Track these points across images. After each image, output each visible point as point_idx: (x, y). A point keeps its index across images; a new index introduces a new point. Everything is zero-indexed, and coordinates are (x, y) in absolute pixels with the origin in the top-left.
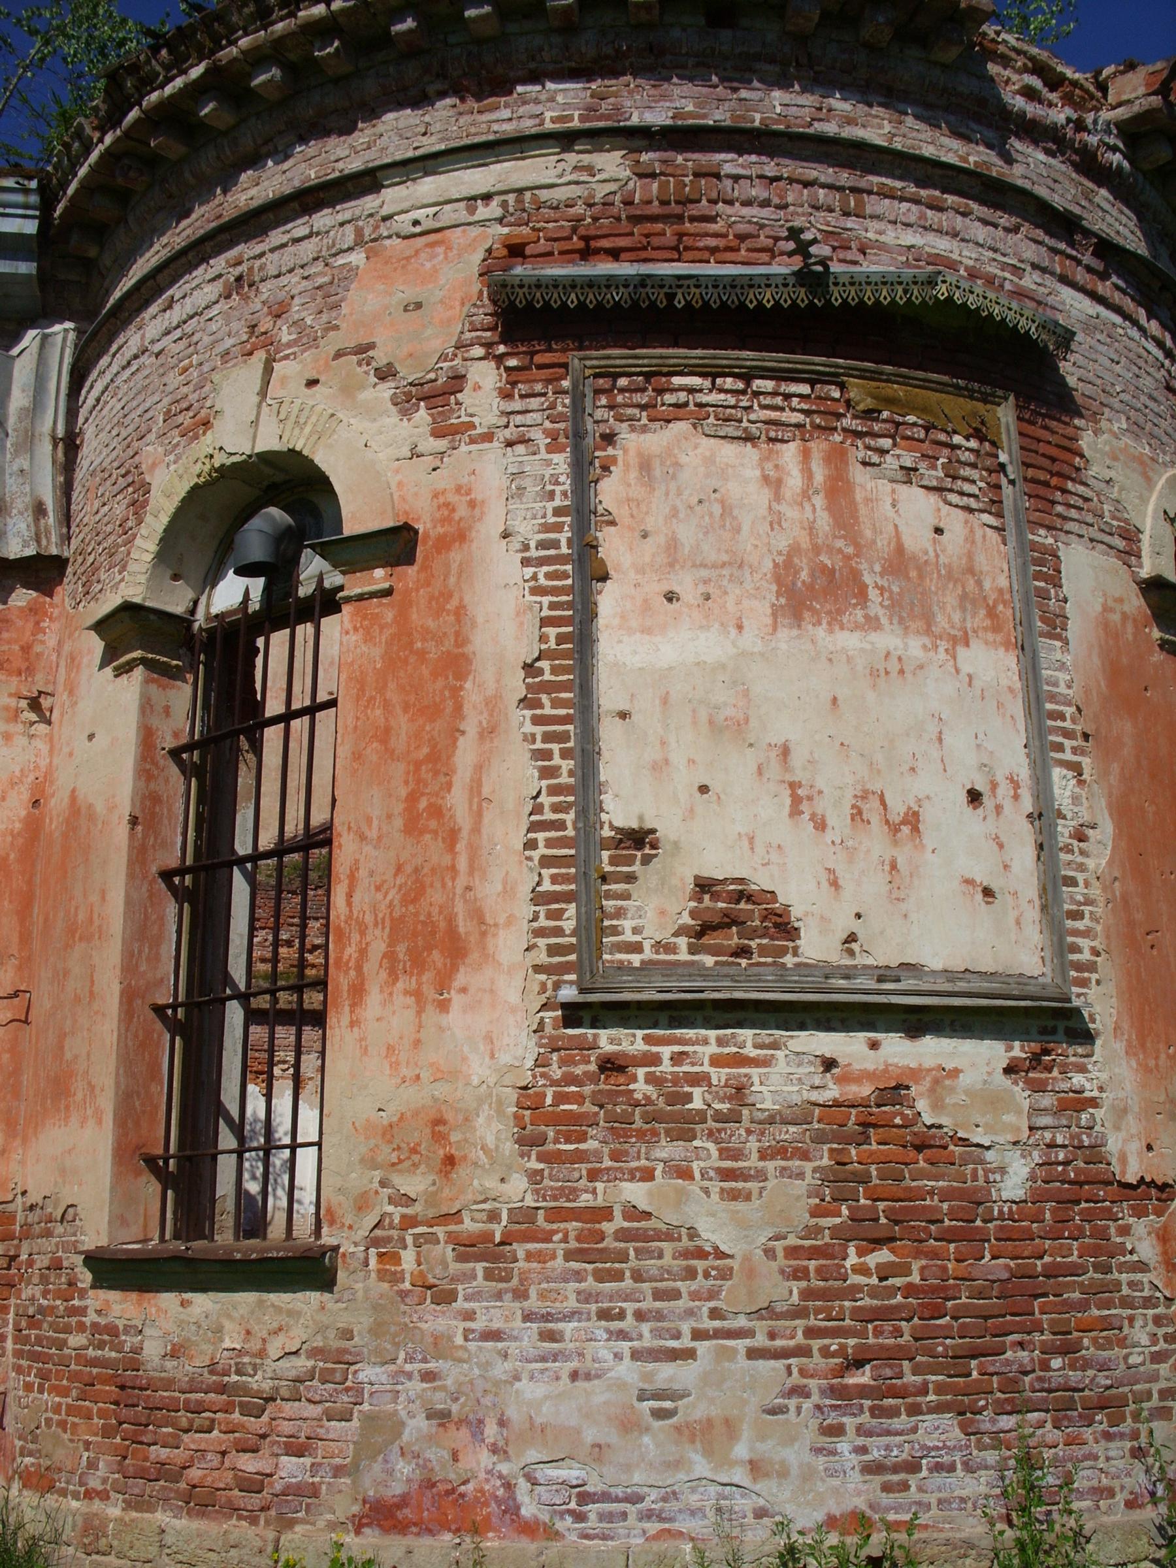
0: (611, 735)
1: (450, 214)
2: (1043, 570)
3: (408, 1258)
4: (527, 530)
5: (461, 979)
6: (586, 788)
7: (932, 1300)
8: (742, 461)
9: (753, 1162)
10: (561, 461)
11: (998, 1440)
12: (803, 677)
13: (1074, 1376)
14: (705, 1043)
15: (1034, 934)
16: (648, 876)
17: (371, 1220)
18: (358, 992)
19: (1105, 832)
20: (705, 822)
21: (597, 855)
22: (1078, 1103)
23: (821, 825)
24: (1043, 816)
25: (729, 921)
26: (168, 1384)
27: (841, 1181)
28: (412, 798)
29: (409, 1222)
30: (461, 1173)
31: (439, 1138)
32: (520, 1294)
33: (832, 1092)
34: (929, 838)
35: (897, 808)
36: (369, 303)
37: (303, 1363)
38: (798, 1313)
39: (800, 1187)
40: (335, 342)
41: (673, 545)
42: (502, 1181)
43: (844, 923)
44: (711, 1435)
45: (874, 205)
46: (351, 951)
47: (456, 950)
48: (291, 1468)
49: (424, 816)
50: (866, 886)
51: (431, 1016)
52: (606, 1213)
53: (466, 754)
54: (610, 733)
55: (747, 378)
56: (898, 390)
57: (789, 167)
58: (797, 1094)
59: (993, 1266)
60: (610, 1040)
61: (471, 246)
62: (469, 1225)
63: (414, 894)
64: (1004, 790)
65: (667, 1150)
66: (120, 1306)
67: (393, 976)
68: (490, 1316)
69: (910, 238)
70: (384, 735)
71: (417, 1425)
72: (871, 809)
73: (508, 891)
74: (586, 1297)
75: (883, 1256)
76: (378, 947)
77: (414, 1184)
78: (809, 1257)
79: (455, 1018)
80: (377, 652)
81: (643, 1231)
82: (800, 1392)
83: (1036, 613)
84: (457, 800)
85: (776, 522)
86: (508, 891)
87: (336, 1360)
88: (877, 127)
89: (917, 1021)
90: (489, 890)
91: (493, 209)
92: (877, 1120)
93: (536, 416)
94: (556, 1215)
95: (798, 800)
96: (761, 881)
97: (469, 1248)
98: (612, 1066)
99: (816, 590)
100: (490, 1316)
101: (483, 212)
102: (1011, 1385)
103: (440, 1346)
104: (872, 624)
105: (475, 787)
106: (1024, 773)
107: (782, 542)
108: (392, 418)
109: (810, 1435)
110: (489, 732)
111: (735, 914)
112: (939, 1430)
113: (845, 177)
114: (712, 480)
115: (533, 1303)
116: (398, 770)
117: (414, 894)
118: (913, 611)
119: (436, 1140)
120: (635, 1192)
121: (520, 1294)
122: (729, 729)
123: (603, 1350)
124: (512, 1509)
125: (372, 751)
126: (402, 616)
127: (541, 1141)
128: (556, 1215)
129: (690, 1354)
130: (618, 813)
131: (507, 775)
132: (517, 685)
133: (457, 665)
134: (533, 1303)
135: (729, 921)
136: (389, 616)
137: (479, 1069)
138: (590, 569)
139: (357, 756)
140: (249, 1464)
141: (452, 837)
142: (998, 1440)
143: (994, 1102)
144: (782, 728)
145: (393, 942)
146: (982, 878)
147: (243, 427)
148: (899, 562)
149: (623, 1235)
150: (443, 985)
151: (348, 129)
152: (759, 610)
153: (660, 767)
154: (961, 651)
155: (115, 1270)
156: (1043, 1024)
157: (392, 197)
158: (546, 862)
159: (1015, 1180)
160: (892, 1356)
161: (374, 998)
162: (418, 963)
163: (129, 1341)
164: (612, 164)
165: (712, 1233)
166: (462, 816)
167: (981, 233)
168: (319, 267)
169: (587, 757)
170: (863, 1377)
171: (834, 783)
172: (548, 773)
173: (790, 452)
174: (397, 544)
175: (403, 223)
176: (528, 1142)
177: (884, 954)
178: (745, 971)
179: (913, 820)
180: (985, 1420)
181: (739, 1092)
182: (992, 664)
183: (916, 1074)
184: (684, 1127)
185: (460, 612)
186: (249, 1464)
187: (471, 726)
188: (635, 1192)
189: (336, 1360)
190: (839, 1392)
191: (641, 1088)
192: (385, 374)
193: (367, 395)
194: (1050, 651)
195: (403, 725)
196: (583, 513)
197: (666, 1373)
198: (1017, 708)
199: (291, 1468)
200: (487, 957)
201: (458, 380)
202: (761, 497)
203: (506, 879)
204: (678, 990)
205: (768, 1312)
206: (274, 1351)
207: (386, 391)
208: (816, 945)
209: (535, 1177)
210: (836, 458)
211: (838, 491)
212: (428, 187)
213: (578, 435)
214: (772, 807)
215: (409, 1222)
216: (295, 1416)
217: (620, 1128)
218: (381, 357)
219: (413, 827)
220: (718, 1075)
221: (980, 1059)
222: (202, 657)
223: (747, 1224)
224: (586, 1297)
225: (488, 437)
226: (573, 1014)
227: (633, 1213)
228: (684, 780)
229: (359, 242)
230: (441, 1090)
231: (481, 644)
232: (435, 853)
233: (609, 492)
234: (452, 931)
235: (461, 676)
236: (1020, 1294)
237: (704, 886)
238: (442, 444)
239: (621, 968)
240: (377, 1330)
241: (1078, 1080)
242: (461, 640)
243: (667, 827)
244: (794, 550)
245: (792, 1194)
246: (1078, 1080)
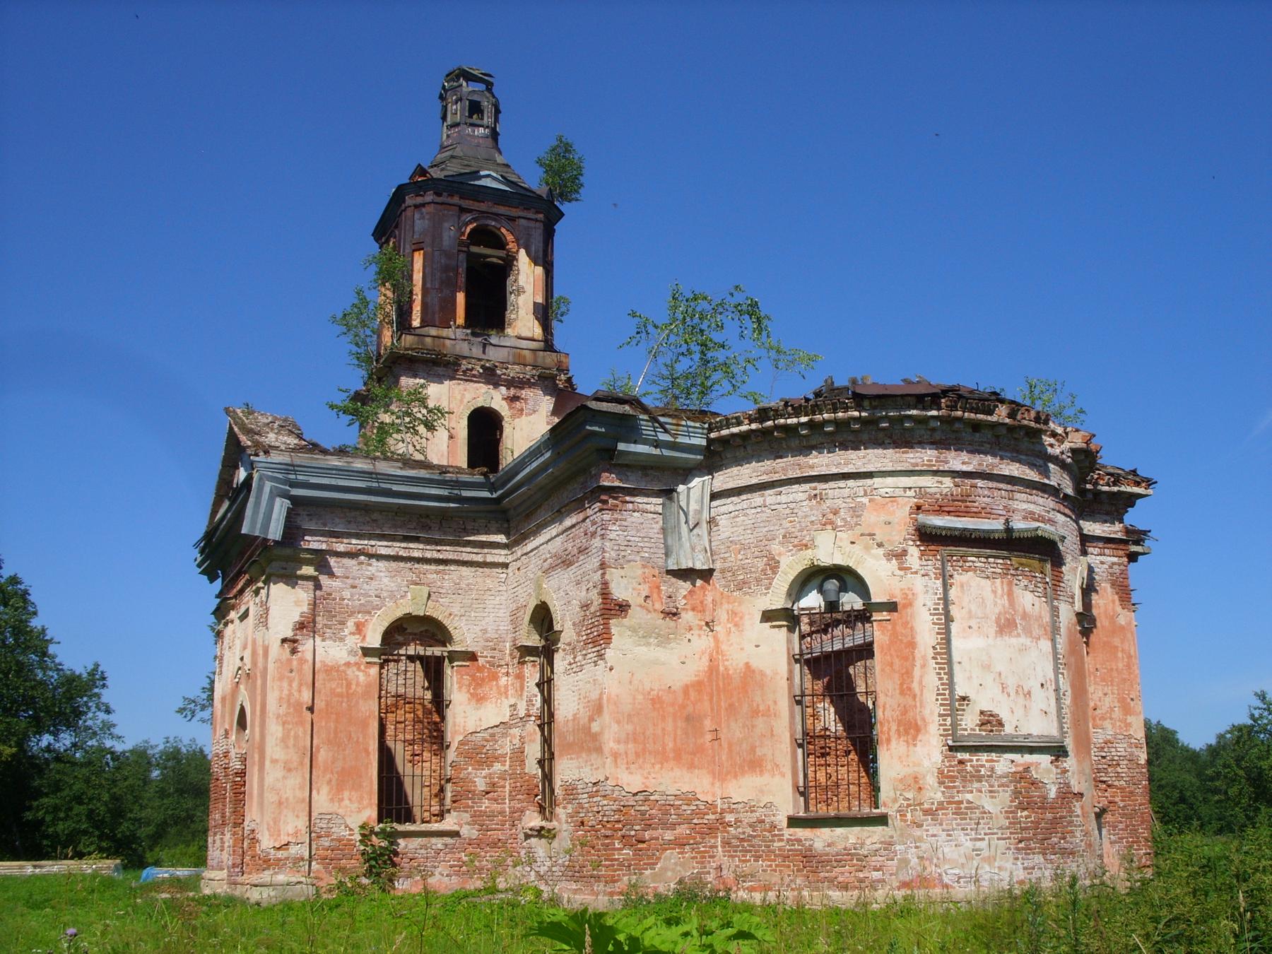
1: (899, 492)
2: (1055, 611)
3: (909, 815)
4: (930, 604)
5: (920, 737)
6: (951, 685)
7: (1036, 824)
9: (996, 788)
10: (939, 583)
11: (1051, 862)
12: (1004, 650)
13: (1066, 846)
14: (984, 757)
15: (1055, 724)
17: (897, 805)
18: (889, 740)
19: (1069, 693)
20: (984, 695)
21: (955, 704)
22: (1065, 771)
24: (1057, 690)
25: (989, 722)
26: (827, 855)
27: (1016, 793)
28: (901, 684)
29: (909, 805)
30: (923, 792)
31: (916, 782)
32: (941, 824)
33: (1014, 770)
35: (1026, 690)
36: (871, 518)
37: (878, 846)
38: (1008, 828)
39: (1007, 795)
40: (858, 530)
41: (970, 612)
42: (935, 794)
44: (990, 860)
45: (1017, 496)
46: (885, 729)
47: (918, 730)
48: (876, 875)
49: (905, 690)
50: (1019, 712)
51: (911, 748)
52: (961, 802)
53: (917, 672)
54: (956, 668)
56: (1024, 560)
57: (995, 485)
58: (1006, 770)
59: (1049, 816)
60: (960, 756)
61: (905, 505)
62: (926, 806)
63: (904, 712)
65: (976, 785)
66: (801, 833)
67: (899, 736)
68: (933, 830)
69: (1025, 506)
70: (891, 664)
71: (914, 861)
73: (932, 713)
74: (958, 825)
75: (1025, 813)
76: (894, 727)
77: (910, 795)
78: (1010, 813)
79: (918, 749)
80: (887, 638)
81: (971, 807)
82: (1009, 849)
84: (915, 686)
86: (932, 713)
87: (888, 845)
88: (1014, 469)
89: (1032, 750)
90: (927, 712)
91: (912, 493)
92: (1023, 778)
93: (932, 565)
94: (949, 803)
95: (1004, 688)
96: (996, 711)
97: (926, 812)
98: (961, 762)
99: (1006, 626)
100: (933, 830)
101: (909, 493)
102: (1053, 848)
103: (920, 839)
104: (1019, 635)
105: (920, 682)
107: (997, 611)
108: (884, 561)
109: (1011, 860)
110: (923, 666)
111: (990, 720)
112: (1039, 859)
113: (1009, 487)
114: (980, 587)
115: (944, 826)
116: (896, 676)
117: (904, 712)
118: (1028, 632)
119: (916, 782)
120: (969, 796)
121: (941, 824)
122: (987, 667)
123: (963, 838)
124: (941, 880)
125: (888, 669)
126: (894, 628)
127: (943, 783)
128: (949, 803)
130: (960, 691)
131: (929, 680)
132: (931, 653)
133: (912, 645)
134: (944, 826)
135: (989, 722)
136: (890, 627)
137: (926, 763)
138: (949, 619)
139: (883, 670)
140: (861, 875)
141: (914, 697)
142: (1051, 862)
143: (1049, 771)
144: (999, 667)
145: (899, 725)
147: (828, 552)
148: (1025, 616)
149: (967, 808)
150: (915, 738)
151: (857, 448)
152: (993, 629)
153: (970, 678)
155: (794, 822)
156: (1059, 752)
157: (877, 481)
158: (942, 705)
159: (1053, 794)
160: (1028, 839)
161: (894, 743)
162: (907, 733)
163: (807, 843)
164: (948, 482)
165: (988, 807)
166: (917, 690)
167: (1041, 501)
168: (849, 500)
169: (950, 674)
170: (1022, 845)
171: (1011, 682)
172: (940, 679)
173: (998, 581)
174: (892, 607)
175: (882, 491)
176: (941, 783)
177: (1024, 732)
178: (994, 739)
179: (1029, 693)
180: (1048, 857)
181: (992, 769)
182: (1046, 645)
184: (979, 779)
185: (912, 629)
186: (861, 875)
187: (918, 663)
188: (969, 796)
189: (888, 845)
190: (1018, 849)
191: (969, 768)
192: (880, 545)
193: (874, 551)
195: (897, 662)
196: (946, 600)
197: (979, 844)
199: (876, 875)
200: (927, 732)
201: (905, 553)
202: (991, 596)
203: (931, 709)
204: (975, 743)
205: (1001, 828)
206: (868, 842)
207: (881, 551)
208: (1008, 729)
209: (943, 793)
210: (1010, 583)
211: (1010, 594)
212: (890, 481)
213: (944, 576)
214: (998, 690)
215: (909, 805)
216: (875, 861)
217: (964, 779)
218: (878, 538)
219: (902, 693)
220: (987, 765)
221: (1045, 760)
223: (995, 803)
224: (958, 825)
225: (916, 573)
226: (951, 749)
227: (969, 802)
228: (976, 682)
229: (866, 494)
230: (916, 769)
231: (919, 639)
232: (910, 701)
233: (953, 593)
234: (916, 724)
235: (914, 648)
236: (1055, 822)
237: (982, 713)
238: (902, 573)
239: (963, 736)
240: (902, 835)
242: (913, 638)
243: (972, 696)
244: (1000, 613)
245: (1005, 796)
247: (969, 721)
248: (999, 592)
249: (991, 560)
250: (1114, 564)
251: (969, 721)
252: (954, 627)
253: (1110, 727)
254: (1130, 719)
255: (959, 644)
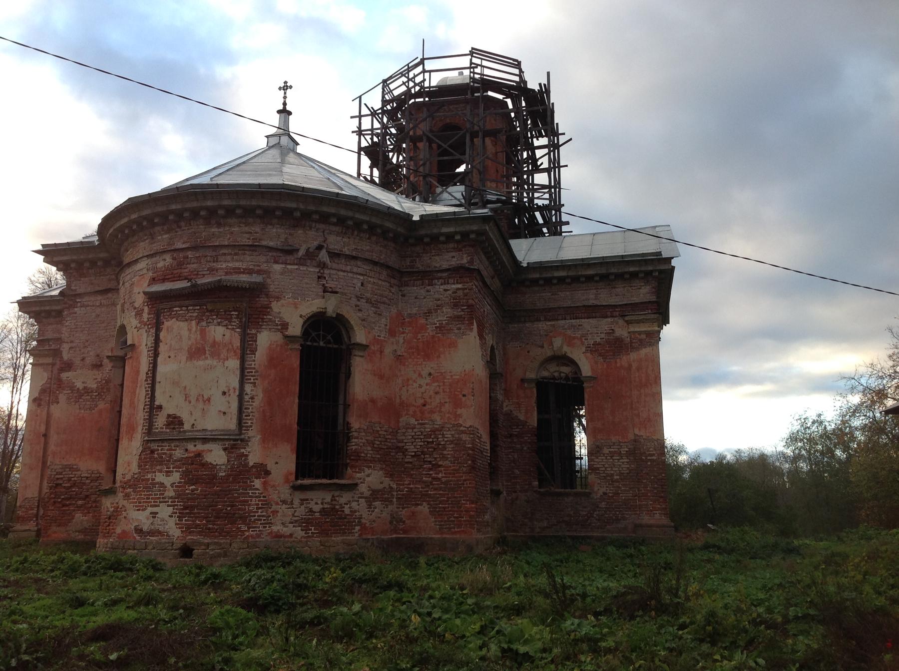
0: (157, 386)
6: (153, 397)
8: (183, 325)
16: (160, 414)
21: (153, 409)
23: (190, 402)
34: (212, 403)
35: (206, 397)
43: (192, 422)
45: (220, 258)
55: (187, 307)
64: (232, 391)
65: (158, 467)
72: (201, 399)
75: (193, 487)
83: (246, 349)
85: (189, 338)
89: (205, 440)
95: (187, 397)
99: (196, 353)
104: (206, 358)
106: (237, 386)
107: (190, 343)
110: (141, 387)
111: (175, 421)
118: (215, 354)
122: (176, 383)
129: (159, 506)
130: (157, 403)
138: (156, 354)
146: (223, 410)
148: (214, 344)
152: (183, 357)
154: (226, 362)
179: (209, 400)
183: (203, 451)
194: (250, 357)
198: (238, 372)
208: (187, 427)
222: (513, 115)
233: (162, 335)
241: (242, 450)
243: (164, 405)
246: (242, 450)
247: (160, 421)
248: (194, 329)
249: (190, 308)
250: (458, 289)
251: (160, 421)
252: (159, 360)
253: (438, 418)
254: (459, 411)
255: (163, 368)
